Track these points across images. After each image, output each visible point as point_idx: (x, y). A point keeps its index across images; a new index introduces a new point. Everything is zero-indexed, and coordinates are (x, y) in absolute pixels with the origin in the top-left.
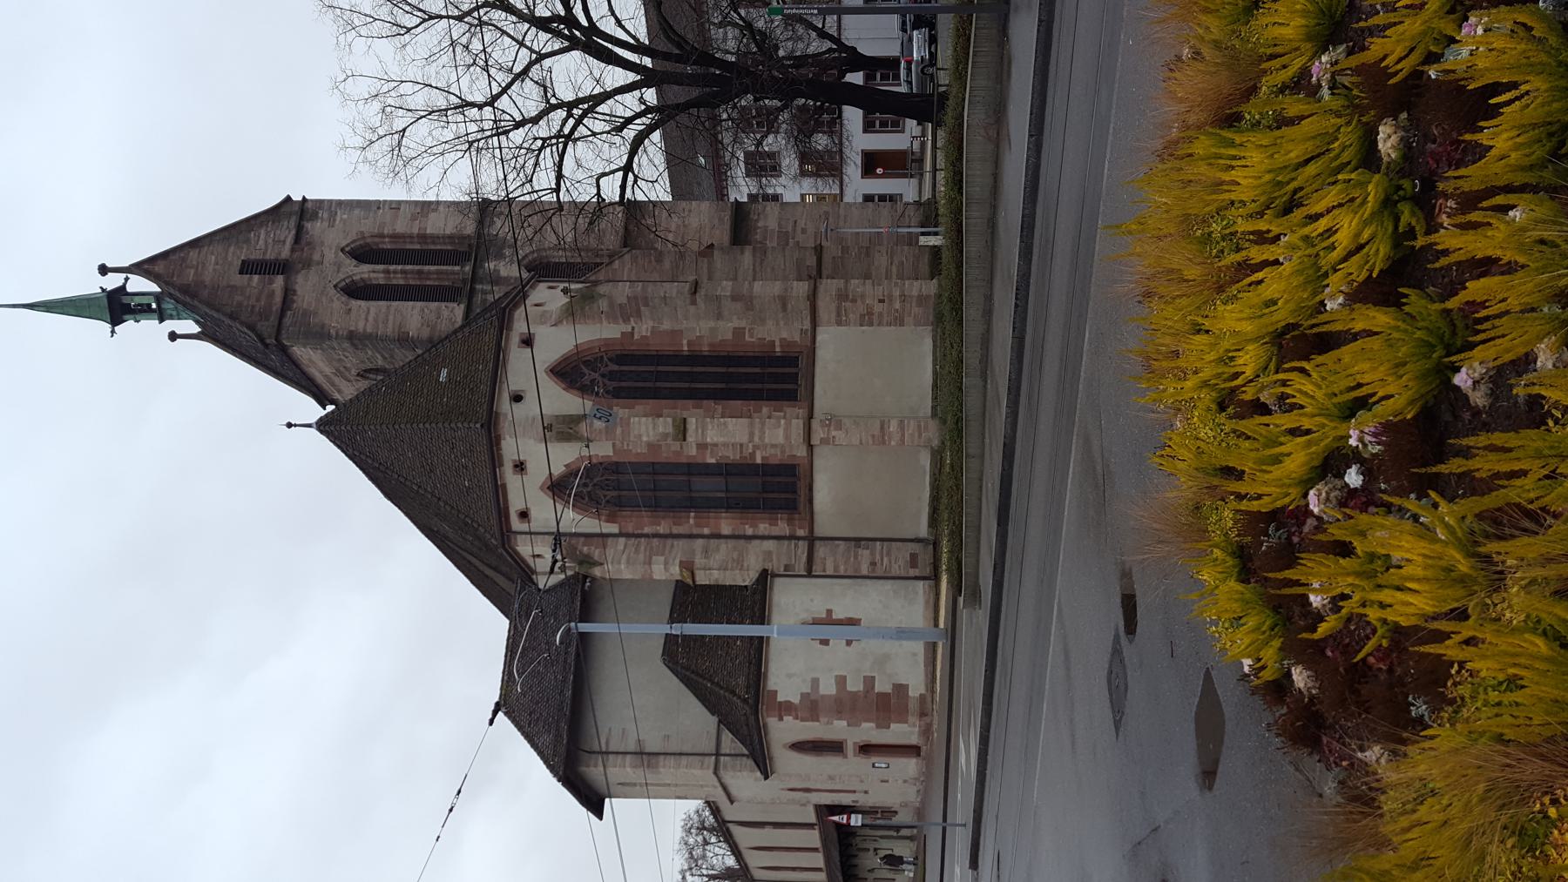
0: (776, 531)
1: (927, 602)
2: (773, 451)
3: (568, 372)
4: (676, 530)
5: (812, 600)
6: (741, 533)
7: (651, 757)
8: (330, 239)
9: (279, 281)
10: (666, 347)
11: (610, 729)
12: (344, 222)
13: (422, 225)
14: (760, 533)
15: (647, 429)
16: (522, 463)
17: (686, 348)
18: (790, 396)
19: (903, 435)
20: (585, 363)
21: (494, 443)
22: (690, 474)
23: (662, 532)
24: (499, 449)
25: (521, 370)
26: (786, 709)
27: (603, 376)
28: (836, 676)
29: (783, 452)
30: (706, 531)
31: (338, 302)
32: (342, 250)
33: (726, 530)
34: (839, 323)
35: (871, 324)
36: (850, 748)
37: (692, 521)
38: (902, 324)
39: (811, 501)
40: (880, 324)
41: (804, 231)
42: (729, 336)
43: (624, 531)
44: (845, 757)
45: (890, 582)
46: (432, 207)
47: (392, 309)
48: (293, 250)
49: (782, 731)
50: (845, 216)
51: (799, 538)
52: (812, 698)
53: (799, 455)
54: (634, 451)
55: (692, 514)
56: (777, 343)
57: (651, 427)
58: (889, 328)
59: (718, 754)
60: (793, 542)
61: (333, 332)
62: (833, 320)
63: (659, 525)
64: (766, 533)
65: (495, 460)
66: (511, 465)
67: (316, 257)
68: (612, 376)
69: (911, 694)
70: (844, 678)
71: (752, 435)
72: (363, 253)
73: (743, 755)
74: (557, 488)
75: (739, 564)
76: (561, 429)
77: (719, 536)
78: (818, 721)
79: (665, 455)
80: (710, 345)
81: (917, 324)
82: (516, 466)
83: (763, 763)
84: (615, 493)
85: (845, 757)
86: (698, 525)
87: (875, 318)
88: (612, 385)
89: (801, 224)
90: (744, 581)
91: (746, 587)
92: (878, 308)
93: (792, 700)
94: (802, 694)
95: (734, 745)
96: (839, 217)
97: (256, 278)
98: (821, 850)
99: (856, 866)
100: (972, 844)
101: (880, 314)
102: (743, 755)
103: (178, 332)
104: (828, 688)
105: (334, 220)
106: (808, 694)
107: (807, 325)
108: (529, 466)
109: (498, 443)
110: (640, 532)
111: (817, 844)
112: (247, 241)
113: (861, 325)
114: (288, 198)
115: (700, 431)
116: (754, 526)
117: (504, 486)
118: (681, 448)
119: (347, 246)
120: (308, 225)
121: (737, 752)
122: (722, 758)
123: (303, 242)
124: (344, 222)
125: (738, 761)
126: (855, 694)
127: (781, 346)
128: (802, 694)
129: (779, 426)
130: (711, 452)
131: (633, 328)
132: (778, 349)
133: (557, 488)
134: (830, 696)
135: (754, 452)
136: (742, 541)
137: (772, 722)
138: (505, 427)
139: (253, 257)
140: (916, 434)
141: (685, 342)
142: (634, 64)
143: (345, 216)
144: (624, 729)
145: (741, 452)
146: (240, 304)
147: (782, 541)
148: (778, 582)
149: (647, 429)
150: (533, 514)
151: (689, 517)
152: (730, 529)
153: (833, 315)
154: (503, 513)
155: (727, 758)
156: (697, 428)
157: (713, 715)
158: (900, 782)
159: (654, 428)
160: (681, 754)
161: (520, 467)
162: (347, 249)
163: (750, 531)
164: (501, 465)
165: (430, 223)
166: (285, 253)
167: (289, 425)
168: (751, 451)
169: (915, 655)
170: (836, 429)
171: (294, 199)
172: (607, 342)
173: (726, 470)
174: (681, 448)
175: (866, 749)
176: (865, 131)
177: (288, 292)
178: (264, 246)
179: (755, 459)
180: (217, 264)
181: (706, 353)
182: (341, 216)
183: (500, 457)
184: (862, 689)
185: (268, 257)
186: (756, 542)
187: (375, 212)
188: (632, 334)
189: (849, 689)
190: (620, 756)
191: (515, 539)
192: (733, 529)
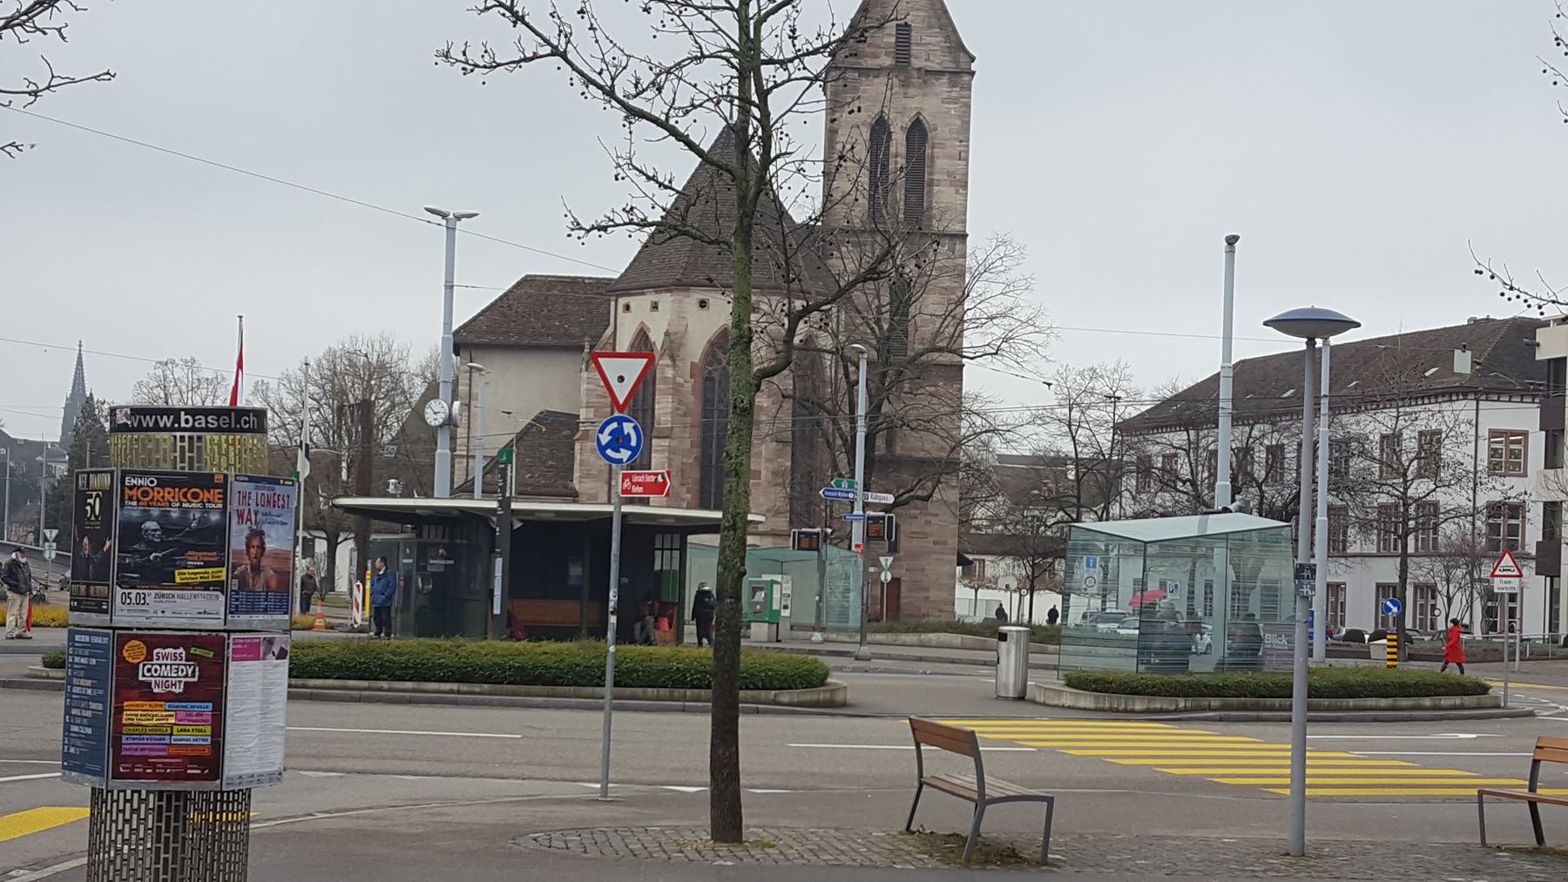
8: (930, 103)
9: (887, 61)
12: (948, 112)
31: (868, 116)
32: (919, 113)
41: (928, 523)
46: (961, 191)
48: (919, 69)
50: (942, 560)
57: (665, 411)
61: (837, 115)
65: (659, 288)
66: (656, 300)
67: (912, 91)
72: (917, 132)
73: (467, 476)
75: (586, 476)
89: (934, 520)
96: (943, 554)
97: (893, 40)
100: (1540, 826)
102: (467, 476)
112: (930, 27)
114: (973, 59)
117: (643, 294)
120: (945, 80)
123: (927, 78)
124: (948, 112)
136: (606, 476)
138: (678, 296)
139: (913, 34)
143: (953, 112)
150: (628, 315)
155: (465, 464)
162: (921, 117)
164: (657, 292)
165: (944, 189)
166: (916, 63)
171: (973, 64)
176: (1378, 586)
177: (877, 71)
182: (953, 109)
185: (913, 47)
186: (606, 488)
187: (955, 139)
190: (468, 382)
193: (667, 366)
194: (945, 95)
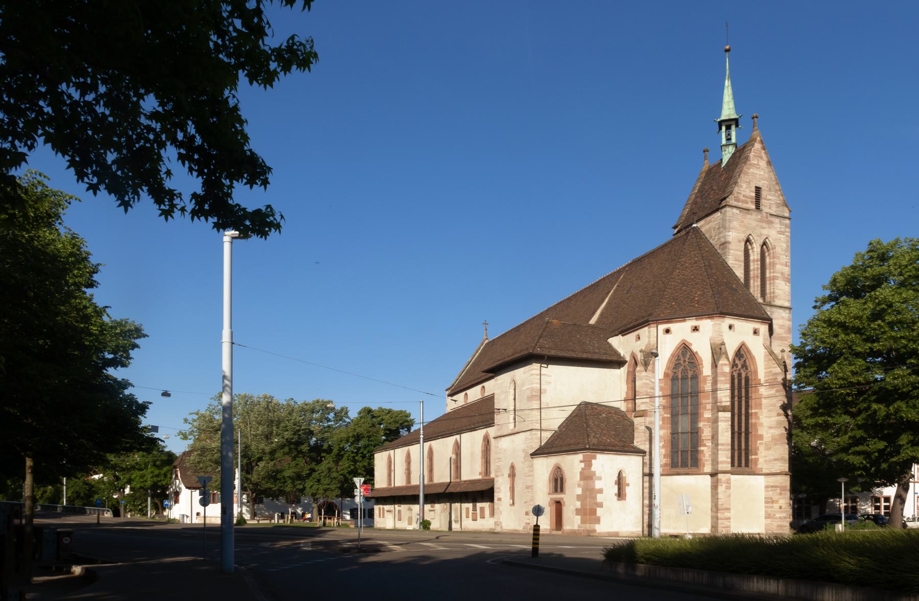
1: (633, 533)
3: (742, 353)
9: (753, 207)
10: (752, 403)
13: (779, 278)
16: (697, 330)
17: (753, 411)
20: (745, 361)
22: (692, 414)
25: (681, 330)
26: (588, 463)
27: (740, 370)
32: (767, 238)
34: (767, 487)
35: (766, 502)
36: (558, 496)
37: (665, 415)
38: (766, 518)
39: (678, 474)
40: (766, 507)
42: (760, 432)
44: (549, 494)
45: (641, 515)
47: (740, 263)
49: (572, 463)
54: (705, 386)
55: (669, 416)
56: (756, 457)
58: (763, 513)
59: (541, 430)
62: (768, 484)
68: (740, 375)
69: (597, 525)
71: (723, 445)
74: (685, 348)
76: (718, 351)
78: (580, 480)
80: (756, 424)
81: (766, 525)
82: (696, 327)
83: (542, 451)
84: (680, 377)
85: (549, 494)
87: (770, 505)
88: (735, 374)
90: (637, 442)
92: (776, 506)
93: (593, 467)
94: (595, 472)
98: (431, 483)
101: (772, 507)
104: (598, 485)
105: (781, 234)
106: (595, 475)
107: (765, 471)
108: (696, 333)
111: (437, 480)
113: (765, 498)
118: (708, 410)
119: (769, 241)
122: (539, 432)
126: (595, 498)
127: (755, 459)
128: (595, 472)
129: (727, 458)
132: (753, 457)
133: (685, 348)
134: (594, 485)
135: (706, 446)
137: (580, 456)
141: (757, 411)
142: (741, 384)
144: (550, 383)
148: (641, 458)
150: (668, 336)
151: (667, 414)
157: (559, 427)
158: (528, 521)
161: (696, 329)
165: (780, 282)
167: (80, 201)
170: (726, 486)
172: (756, 372)
173: (695, 433)
174: (708, 410)
180: (760, 175)
191: (654, 327)
193: (726, 365)
194: (779, 230)
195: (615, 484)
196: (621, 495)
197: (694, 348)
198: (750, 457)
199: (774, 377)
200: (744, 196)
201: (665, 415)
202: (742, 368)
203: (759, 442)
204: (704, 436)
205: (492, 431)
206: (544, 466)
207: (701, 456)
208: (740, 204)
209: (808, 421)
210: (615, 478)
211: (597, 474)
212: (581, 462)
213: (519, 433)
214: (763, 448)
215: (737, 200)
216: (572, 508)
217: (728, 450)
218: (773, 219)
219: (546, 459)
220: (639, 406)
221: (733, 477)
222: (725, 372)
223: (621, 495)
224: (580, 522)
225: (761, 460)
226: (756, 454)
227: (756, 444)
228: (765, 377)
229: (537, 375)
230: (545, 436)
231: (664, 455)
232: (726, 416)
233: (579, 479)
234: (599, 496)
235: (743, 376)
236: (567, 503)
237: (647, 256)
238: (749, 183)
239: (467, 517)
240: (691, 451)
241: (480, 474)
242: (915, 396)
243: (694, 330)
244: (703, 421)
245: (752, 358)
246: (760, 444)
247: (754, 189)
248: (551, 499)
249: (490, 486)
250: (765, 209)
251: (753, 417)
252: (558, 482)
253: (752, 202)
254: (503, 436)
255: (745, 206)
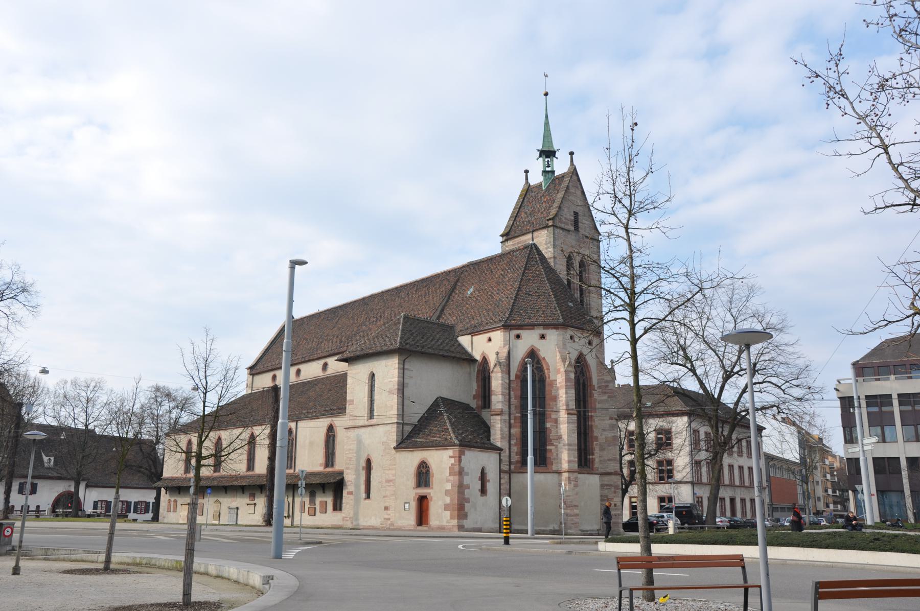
0: (513, 455)
2: (555, 454)
4: (513, 408)
5: (492, 472)
6: (511, 438)
7: (402, 391)
9: (573, 228)
11: (412, 371)
14: (512, 447)
15: (571, 397)
16: (544, 338)
17: (589, 414)
18: (580, 465)
19: (573, 516)
21: (555, 326)
23: (511, 400)
24: (552, 329)
28: (469, 484)
29: (554, 459)
30: (512, 421)
33: (513, 431)
36: (423, 491)
42: (595, 434)
43: (511, 382)
44: (414, 489)
51: (510, 466)
52: (463, 473)
53: (553, 467)
55: (520, 415)
57: (571, 399)
60: (508, 463)
62: (603, 483)
63: (515, 399)
64: (512, 450)
65: (546, 326)
69: (465, 521)
70: (469, 488)
77: (510, 427)
78: (450, 475)
79: (551, 403)
80: (592, 426)
82: (543, 335)
86: (515, 418)
91: (490, 440)
95: (406, 432)
99: (262, 493)
103: (528, 174)
108: (543, 341)
109: (555, 328)
110: (511, 390)
115: (571, 421)
116: (516, 444)
121: (404, 435)
122: (401, 426)
125: (400, 434)
129: (575, 458)
130: (553, 425)
131: (596, 390)
132: (591, 457)
135: (554, 445)
140: (573, 522)
145: (553, 439)
146: (563, 211)
147: (508, 457)
149: (571, 397)
152: (514, 433)
153: (606, 483)
154: (520, 327)
156: (572, 420)
158: (387, 517)
159: (571, 400)
160: (403, 405)
161: (543, 337)
163: (513, 442)
164: (544, 329)
168: (554, 444)
169: (477, 523)
170: (574, 485)
172: (591, 378)
175: (422, 502)
178: (584, 222)
179: (549, 446)
181: (587, 424)
183: (548, 329)
184: (466, 497)
188: (594, 390)
189: (466, 490)
192: (513, 435)
195: (479, 480)
196: (483, 491)
197: (542, 354)
198: (588, 457)
199: (606, 384)
200: (566, 218)
201: (517, 415)
202: (580, 374)
203: (595, 443)
204: (552, 436)
205: (339, 422)
206: (412, 459)
207: (548, 455)
208: (563, 226)
209: (819, 492)
210: (479, 474)
211: (466, 470)
212: (451, 457)
213: (378, 425)
214: (598, 449)
215: (561, 221)
216: (440, 503)
217: (575, 450)
218: (587, 240)
219: (410, 453)
220: (495, 405)
221: (580, 476)
222: (571, 379)
223: (483, 491)
224: (449, 518)
225: (597, 460)
226: (593, 454)
227: (592, 445)
228: (598, 383)
229: (407, 369)
230: (407, 429)
231: (516, 453)
232: (573, 418)
233: (448, 475)
234: (466, 491)
235: (581, 381)
236: (434, 498)
237: (483, 262)
238: (568, 208)
239: (750, 469)
240: (540, 449)
241: (321, 465)
242: (684, 353)
243: (541, 338)
244: (550, 422)
245: (587, 365)
246: (596, 444)
247: (572, 214)
248: (416, 494)
249: (340, 478)
250: (581, 231)
251: (590, 419)
252: (423, 475)
253: (571, 224)
254: (358, 427)
255: (566, 227)
